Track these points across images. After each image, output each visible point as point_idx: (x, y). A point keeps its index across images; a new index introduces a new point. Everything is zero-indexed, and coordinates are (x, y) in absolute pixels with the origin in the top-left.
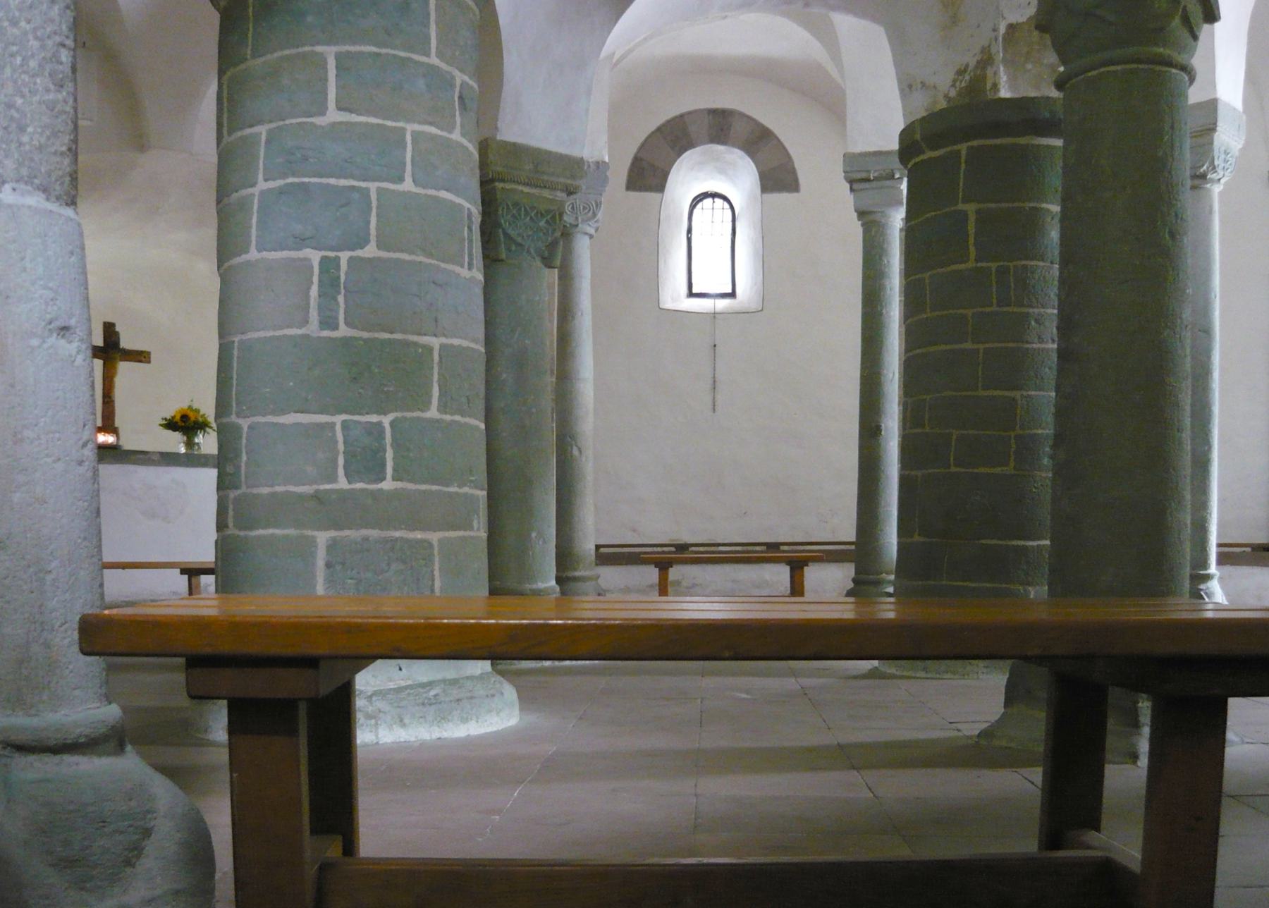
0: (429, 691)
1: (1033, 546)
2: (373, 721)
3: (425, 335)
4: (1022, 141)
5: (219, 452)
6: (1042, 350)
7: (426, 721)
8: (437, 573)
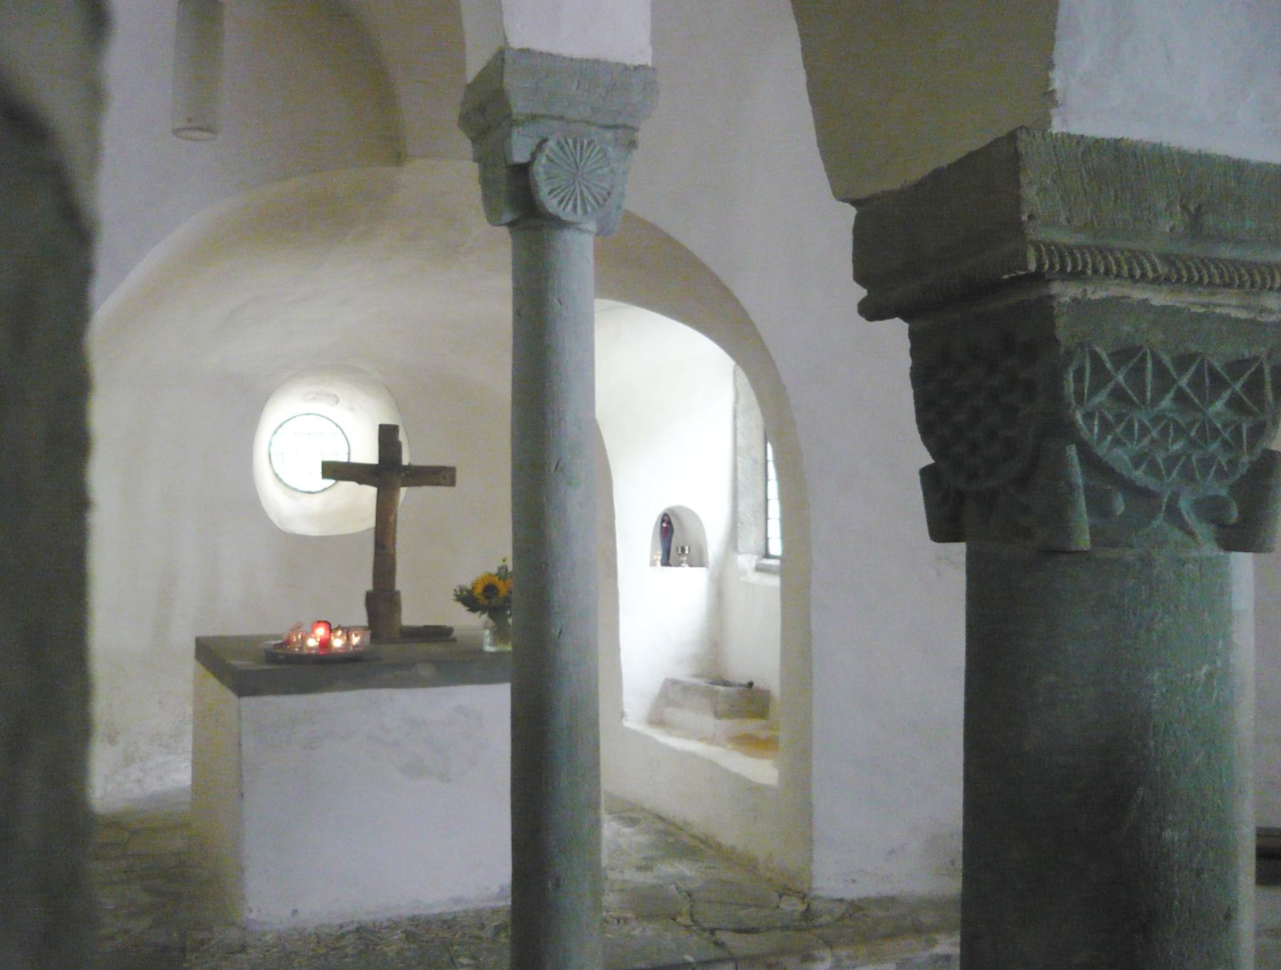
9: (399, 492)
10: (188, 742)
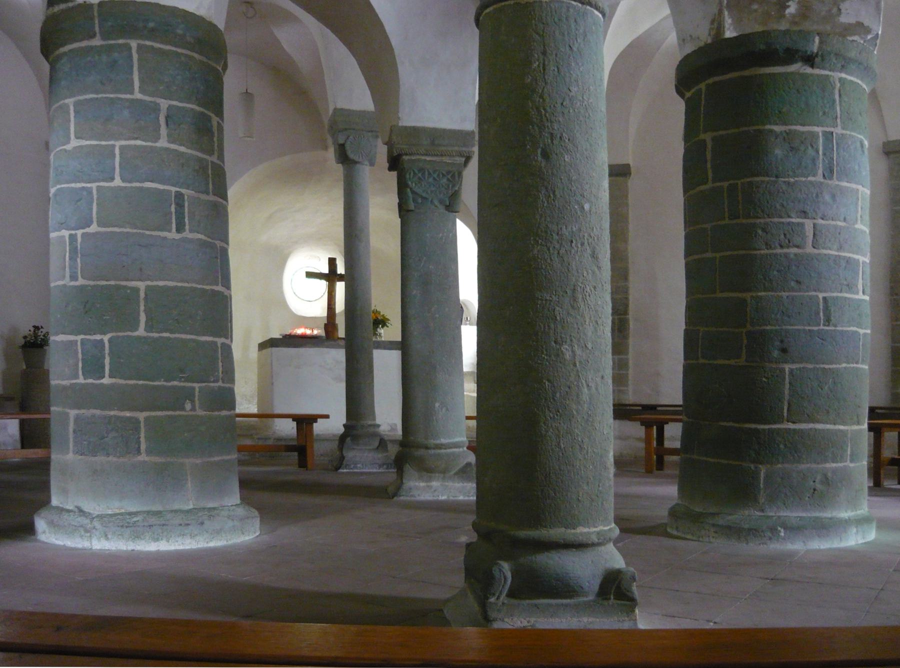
0: (133, 518)
1: (764, 430)
2: (89, 534)
3: (132, 280)
4: (746, 73)
5: (402, 339)
6: (770, 256)
7: (123, 538)
8: (142, 440)
9: (336, 284)
10: (256, 401)
